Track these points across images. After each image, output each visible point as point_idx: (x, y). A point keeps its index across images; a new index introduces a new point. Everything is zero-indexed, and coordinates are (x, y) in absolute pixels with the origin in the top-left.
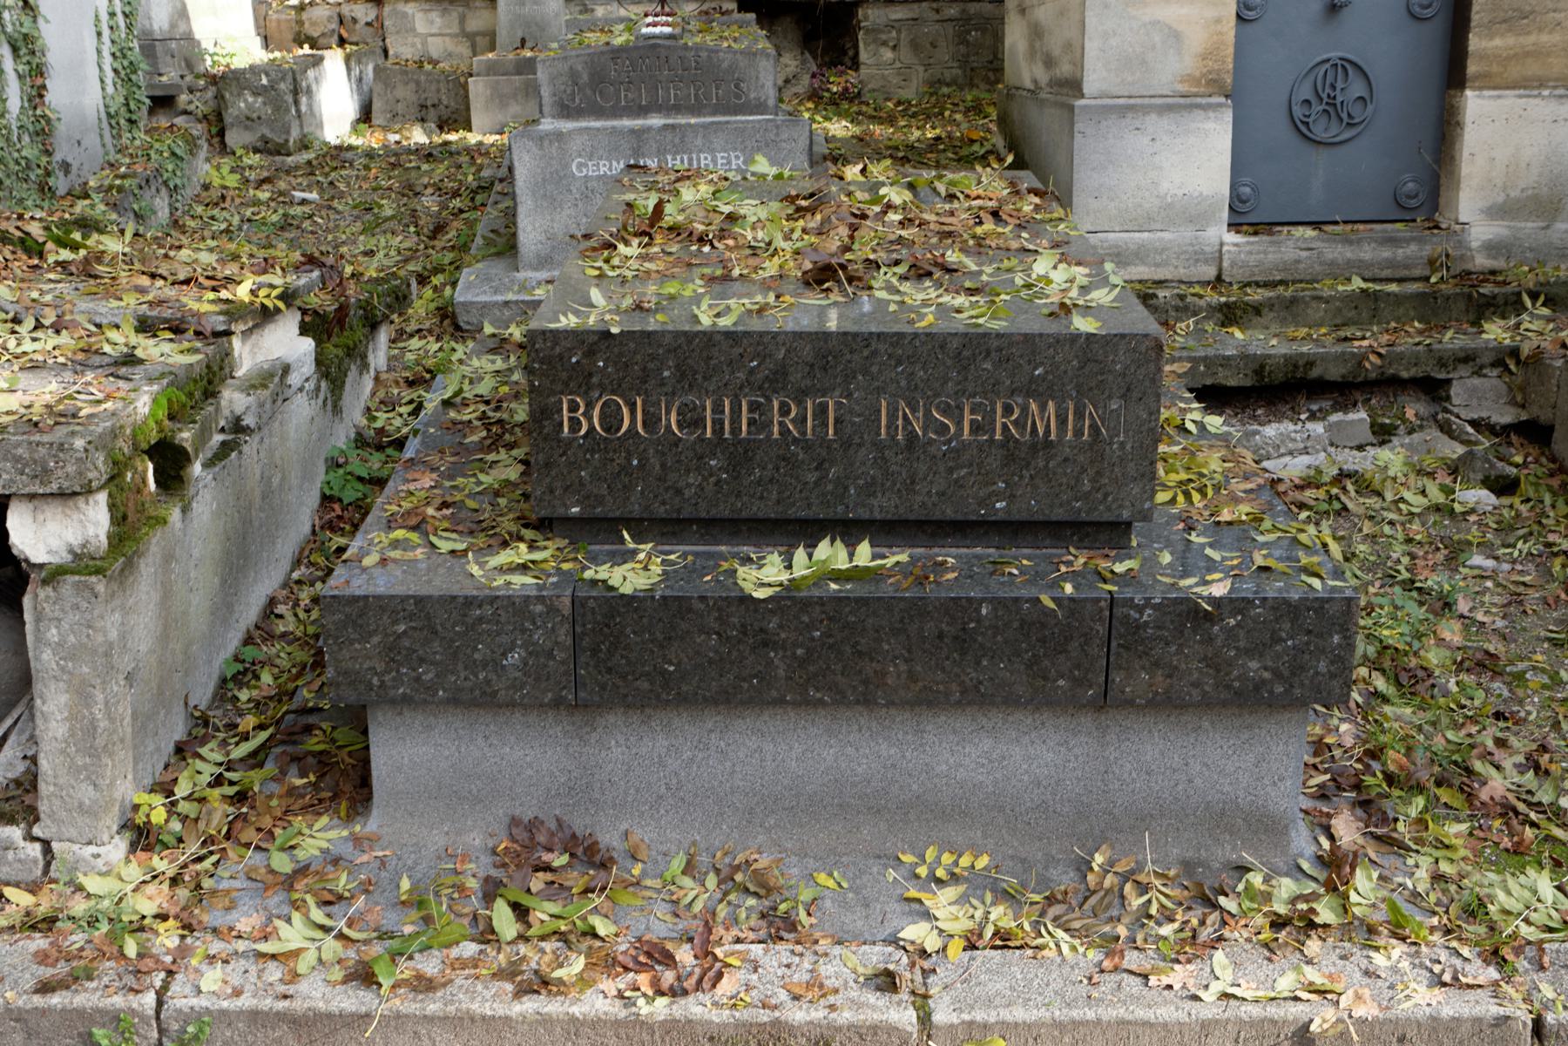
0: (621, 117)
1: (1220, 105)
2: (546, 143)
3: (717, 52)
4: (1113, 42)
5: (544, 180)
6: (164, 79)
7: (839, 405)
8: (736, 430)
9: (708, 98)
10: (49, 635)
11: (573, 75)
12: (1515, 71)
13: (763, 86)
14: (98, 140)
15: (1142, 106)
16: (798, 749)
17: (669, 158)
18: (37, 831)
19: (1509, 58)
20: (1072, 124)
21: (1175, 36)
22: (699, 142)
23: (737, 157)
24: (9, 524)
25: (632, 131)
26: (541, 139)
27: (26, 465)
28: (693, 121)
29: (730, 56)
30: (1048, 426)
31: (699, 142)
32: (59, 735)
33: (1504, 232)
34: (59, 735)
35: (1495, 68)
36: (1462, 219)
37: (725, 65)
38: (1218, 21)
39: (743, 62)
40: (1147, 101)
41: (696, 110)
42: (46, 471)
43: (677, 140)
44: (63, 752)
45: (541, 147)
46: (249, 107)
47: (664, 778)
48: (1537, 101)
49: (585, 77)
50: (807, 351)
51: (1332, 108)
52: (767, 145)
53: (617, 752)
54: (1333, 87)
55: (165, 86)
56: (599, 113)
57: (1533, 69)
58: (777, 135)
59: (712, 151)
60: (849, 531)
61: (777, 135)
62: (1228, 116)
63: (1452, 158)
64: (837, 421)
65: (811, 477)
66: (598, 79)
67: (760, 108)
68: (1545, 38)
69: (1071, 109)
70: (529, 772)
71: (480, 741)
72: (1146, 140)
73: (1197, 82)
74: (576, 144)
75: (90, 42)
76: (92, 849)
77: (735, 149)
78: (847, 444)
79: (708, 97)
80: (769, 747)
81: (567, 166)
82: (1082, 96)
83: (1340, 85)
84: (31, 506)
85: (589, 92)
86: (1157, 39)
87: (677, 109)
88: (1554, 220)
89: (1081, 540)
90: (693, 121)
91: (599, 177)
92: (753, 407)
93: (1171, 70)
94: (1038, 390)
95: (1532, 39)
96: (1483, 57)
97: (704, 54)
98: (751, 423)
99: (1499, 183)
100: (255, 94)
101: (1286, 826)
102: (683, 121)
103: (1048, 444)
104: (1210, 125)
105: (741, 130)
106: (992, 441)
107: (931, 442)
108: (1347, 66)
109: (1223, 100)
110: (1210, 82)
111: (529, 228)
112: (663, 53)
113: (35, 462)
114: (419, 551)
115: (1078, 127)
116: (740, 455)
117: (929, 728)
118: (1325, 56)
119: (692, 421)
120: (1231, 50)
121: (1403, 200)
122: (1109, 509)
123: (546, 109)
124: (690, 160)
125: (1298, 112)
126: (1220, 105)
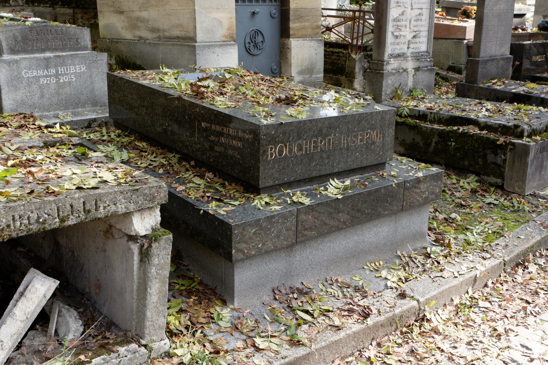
0: (35, 53)
1: (234, 44)
2: (11, 65)
4: (204, 25)
5: (12, 79)
10: (155, 262)
11: (15, 37)
12: (300, 33)
15: (214, 45)
16: (338, 243)
17: (59, 68)
18: (143, 342)
19: (299, 29)
20: (195, 51)
21: (220, 23)
22: (69, 62)
23: (83, 67)
24: (160, 218)
25: (45, 59)
27: (147, 197)
28: (64, 54)
31: (69, 62)
32: (155, 301)
33: (302, 78)
34: (155, 301)
35: (296, 32)
36: (293, 76)
37: (72, 33)
38: (231, 18)
40: (214, 43)
41: (63, 50)
42: (154, 197)
43: (62, 61)
44: (155, 307)
45: (10, 66)
48: (306, 41)
49: (20, 38)
50: (327, 123)
51: (256, 46)
52: (93, 62)
54: (255, 38)
56: (26, 52)
57: (304, 32)
58: (96, 58)
59: (74, 65)
61: (96, 58)
62: (236, 47)
63: (287, 58)
64: (333, 143)
65: (327, 161)
66: (25, 39)
67: (85, 48)
68: (306, 24)
69: (194, 46)
70: (276, 271)
71: (265, 265)
72: (216, 56)
73: (226, 37)
74: (24, 64)
78: (334, 150)
80: (332, 245)
81: (20, 73)
82: (196, 42)
83: (256, 37)
84: (139, 213)
85: (21, 44)
86: (216, 23)
87: (56, 49)
88: (312, 74)
90: (64, 54)
91: (34, 77)
92: (315, 142)
93: (220, 33)
95: (303, 24)
96: (293, 29)
98: (314, 146)
99: (300, 64)
104: (232, 50)
108: (258, 32)
109: (234, 43)
110: (231, 37)
111: (7, 99)
113: (151, 194)
115: (197, 52)
116: (310, 157)
118: (253, 29)
119: (300, 149)
120: (235, 27)
121: (273, 71)
124: (67, 68)
125: (247, 45)
126: (234, 44)
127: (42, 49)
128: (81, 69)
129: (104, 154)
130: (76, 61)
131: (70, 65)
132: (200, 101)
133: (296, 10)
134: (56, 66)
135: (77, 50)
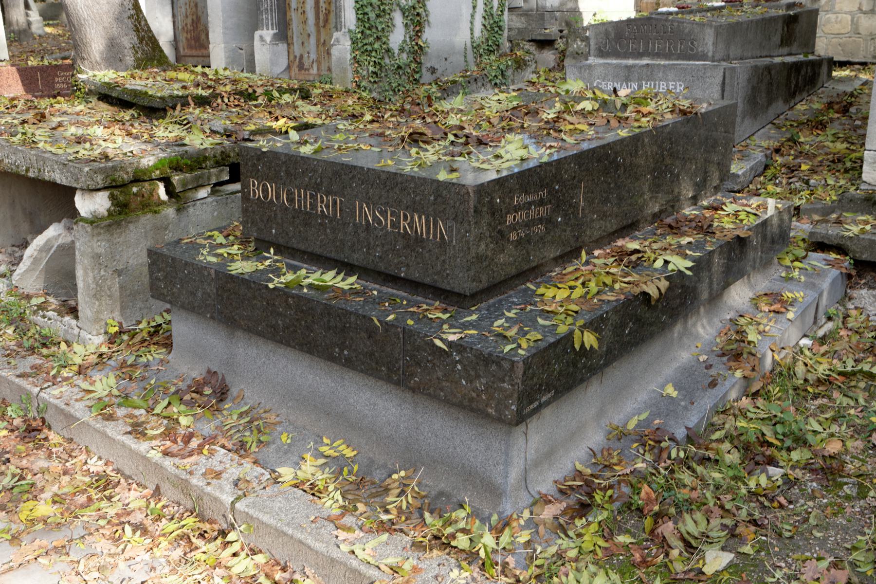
2: (583, 70)
3: (683, 23)
6: (547, 31)
7: (341, 201)
8: (305, 206)
9: (676, 50)
13: (706, 44)
14: (463, 59)
22: (660, 75)
23: (680, 85)
26: (581, 68)
29: (689, 25)
30: (422, 230)
31: (660, 75)
37: (687, 31)
39: (697, 29)
41: (668, 57)
43: (649, 73)
45: (580, 73)
46: (578, 47)
47: (267, 371)
49: (613, 35)
53: (241, 350)
55: (548, 34)
56: (617, 55)
59: (667, 80)
60: (347, 268)
61: (704, 73)
67: (704, 57)
74: (598, 72)
75: (467, 11)
76: (90, 336)
77: (680, 80)
79: (675, 48)
85: (613, 43)
89: (445, 299)
92: (312, 196)
94: (414, 207)
97: (676, 24)
100: (582, 41)
101: (501, 494)
102: (658, 63)
103: (422, 240)
105: (684, 70)
106: (399, 232)
107: (375, 228)
112: (654, 22)
114: (236, 247)
117: (346, 377)
122: (449, 283)
123: (592, 52)
124: (655, 85)
127: (639, 53)
128: (676, 88)
129: (142, 564)
130: (671, 75)
131: (661, 80)
132: (575, 459)
133: (638, 11)
134: (640, 79)
135: (690, 58)
